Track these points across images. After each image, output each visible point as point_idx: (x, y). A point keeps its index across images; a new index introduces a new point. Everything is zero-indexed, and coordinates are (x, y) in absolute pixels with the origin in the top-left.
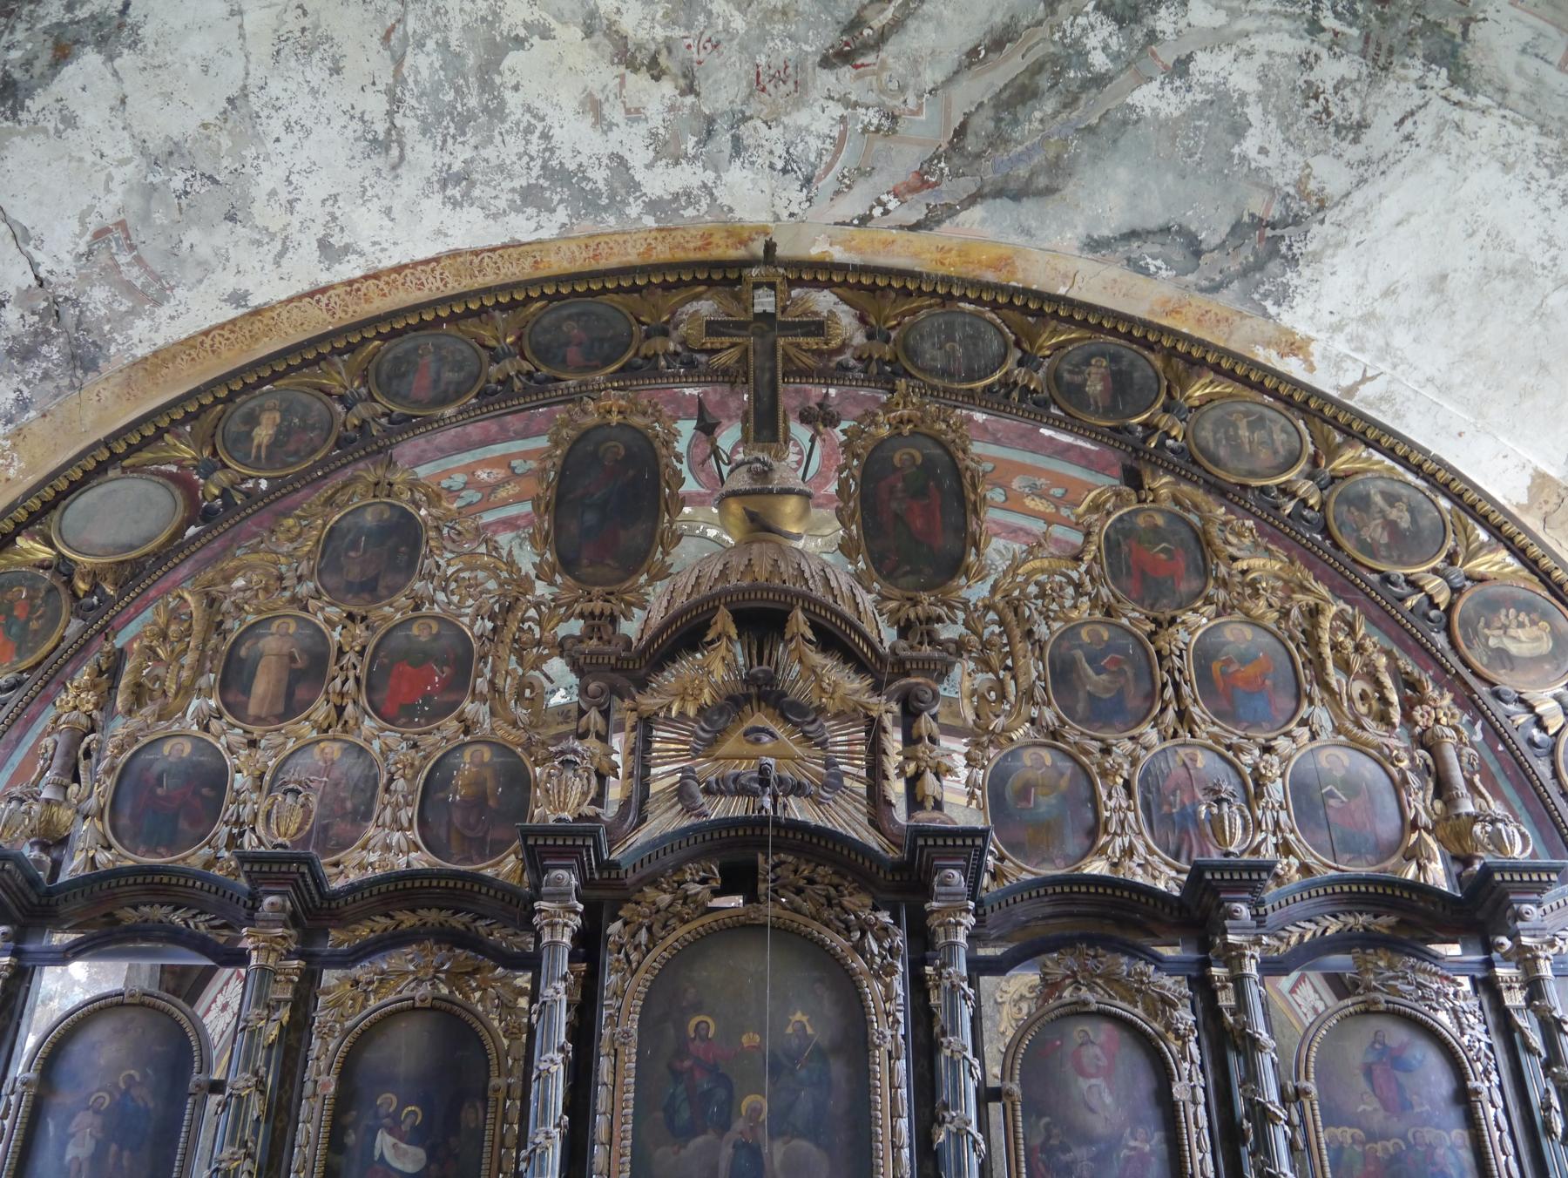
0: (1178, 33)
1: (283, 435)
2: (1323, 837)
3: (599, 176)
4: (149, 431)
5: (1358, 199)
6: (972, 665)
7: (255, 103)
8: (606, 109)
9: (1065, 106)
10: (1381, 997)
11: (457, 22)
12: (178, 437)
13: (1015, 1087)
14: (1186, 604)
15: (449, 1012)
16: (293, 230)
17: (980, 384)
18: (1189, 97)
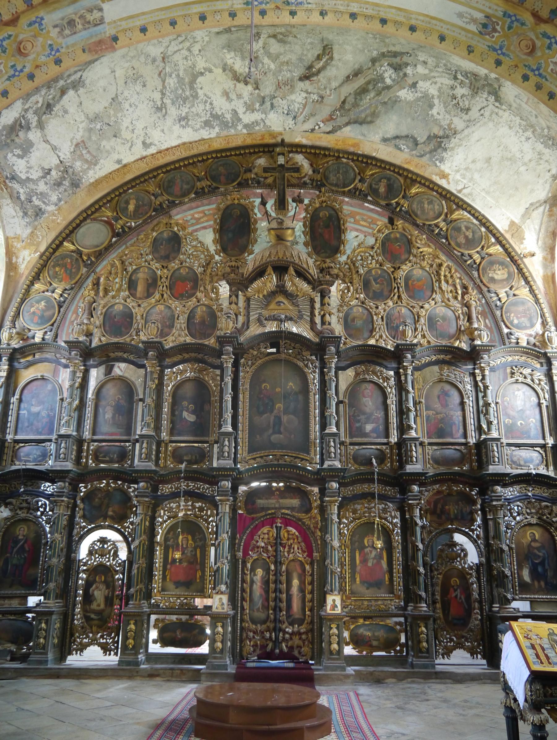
0: (413, 74)
1: (137, 207)
2: (435, 333)
3: (228, 116)
4: (97, 207)
5: (466, 132)
6: (340, 282)
7: (120, 99)
8: (230, 95)
9: (377, 95)
10: (444, 377)
11: (182, 68)
12: (106, 208)
13: (346, 401)
14: (403, 263)
15: (199, 381)
16: (134, 139)
17: (347, 189)
18: (416, 95)
